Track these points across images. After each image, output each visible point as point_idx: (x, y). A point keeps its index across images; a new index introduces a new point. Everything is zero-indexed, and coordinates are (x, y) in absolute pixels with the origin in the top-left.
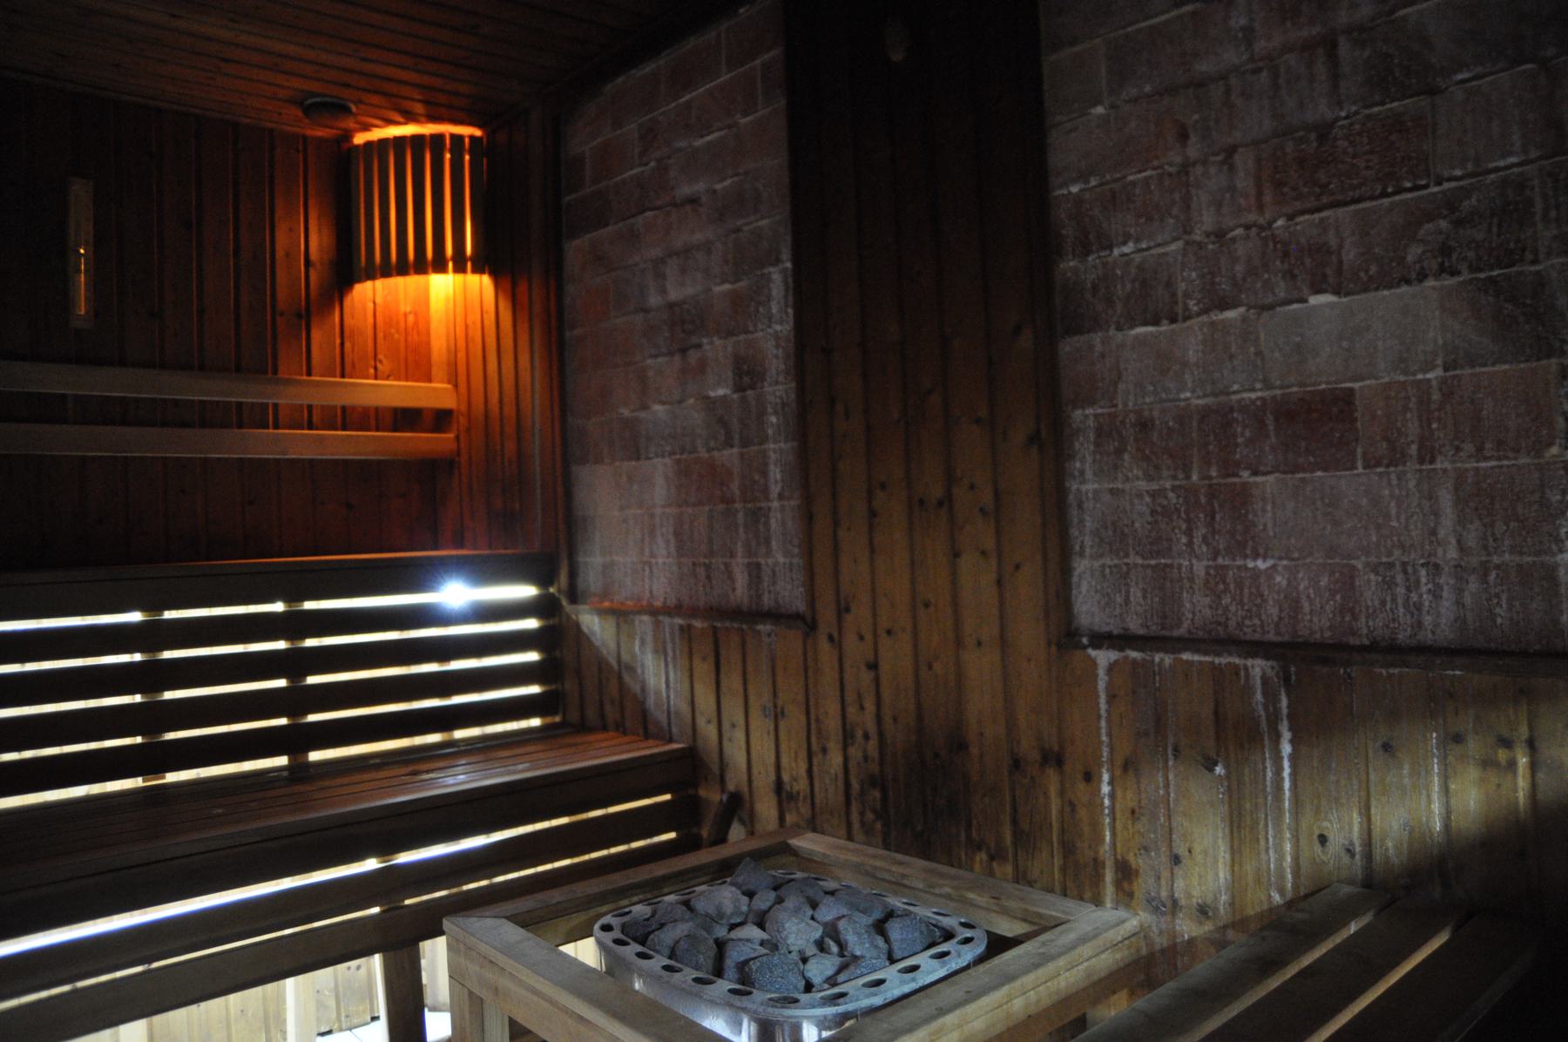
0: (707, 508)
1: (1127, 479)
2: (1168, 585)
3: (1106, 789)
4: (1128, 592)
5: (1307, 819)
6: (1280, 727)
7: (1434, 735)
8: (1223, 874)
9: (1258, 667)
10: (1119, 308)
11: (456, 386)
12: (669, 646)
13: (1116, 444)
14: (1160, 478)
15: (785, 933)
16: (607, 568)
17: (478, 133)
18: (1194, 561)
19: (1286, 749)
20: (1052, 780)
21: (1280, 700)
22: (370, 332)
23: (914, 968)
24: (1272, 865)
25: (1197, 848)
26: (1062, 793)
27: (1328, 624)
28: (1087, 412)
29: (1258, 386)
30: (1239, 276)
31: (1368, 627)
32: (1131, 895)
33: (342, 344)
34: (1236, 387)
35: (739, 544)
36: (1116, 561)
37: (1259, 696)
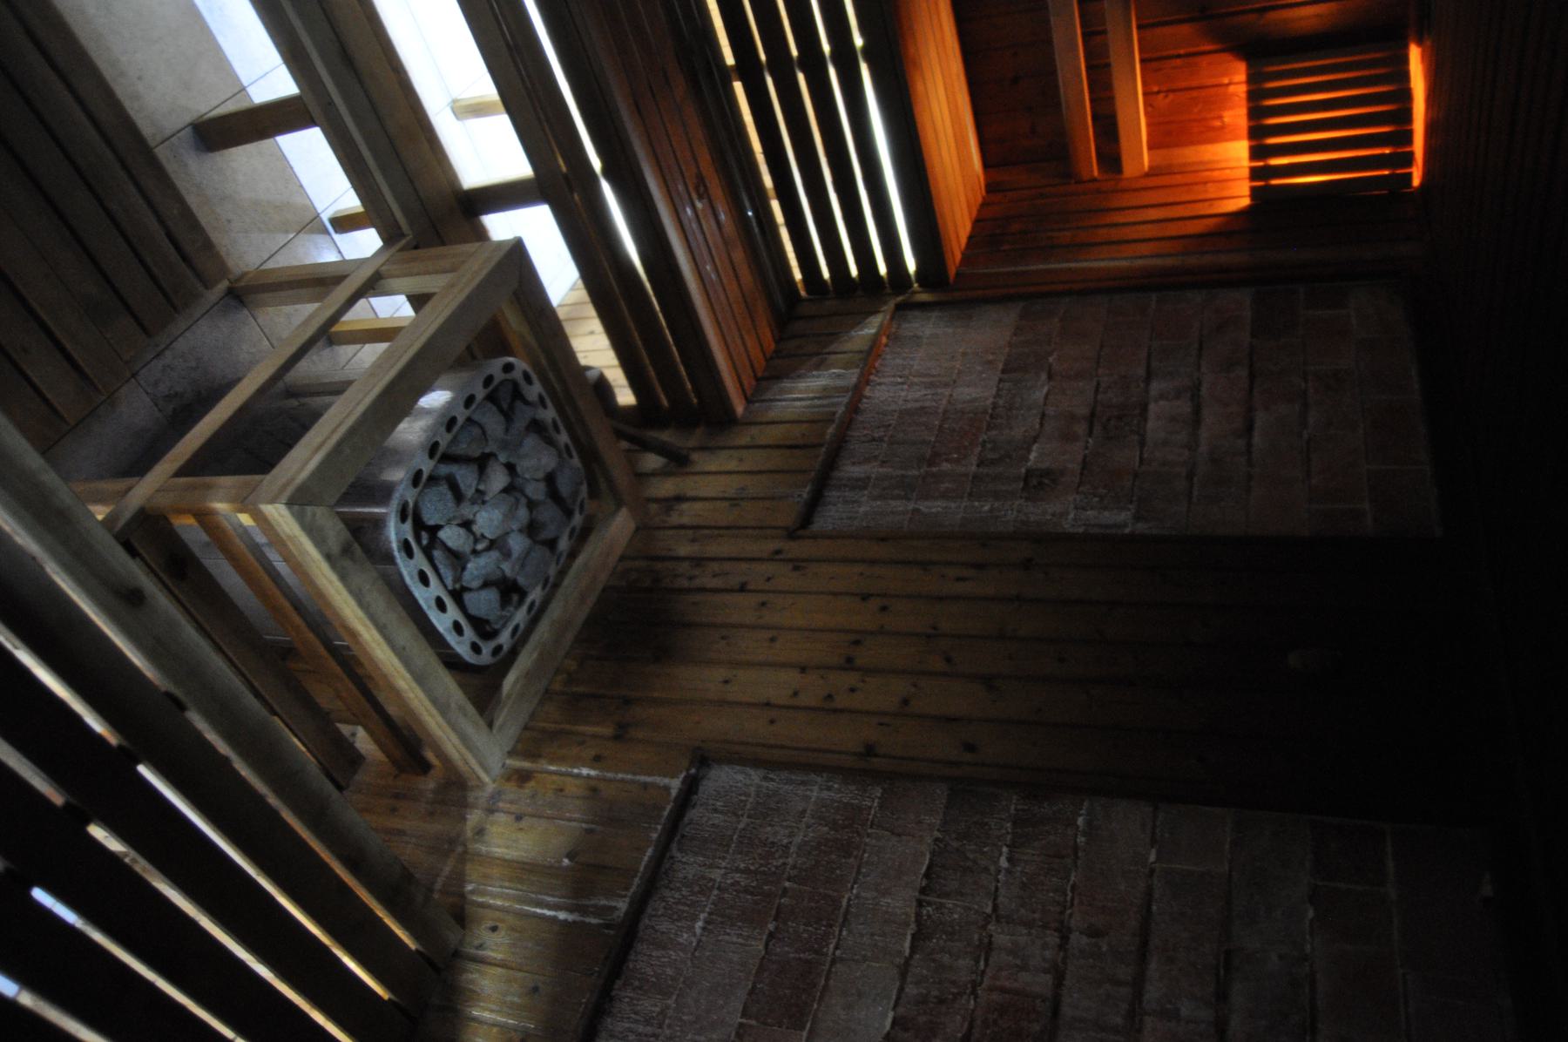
1: (808, 827)
2: (714, 847)
3: (585, 771)
4: (721, 812)
5: (510, 919)
6: (577, 914)
7: (532, 1026)
8: (498, 851)
9: (622, 905)
10: (955, 844)
11: (1147, 175)
12: (825, 402)
13: (840, 822)
14: (798, 855)
16: (917, 339)
17: (1416, 182)
18: (723, 871)
19: (562, 915)
20: (607, 730)
21: (595, 918)
22: (1195, 83)
24: (490, 888)
25: (520, 835)
26: (594, 736)
27: (638, 967)
28: (876, 801)
29: (838, 953)
30: (938, 957)
31: (624, 998)
32: (508, 779)
33: (1179, 56)
34: (844, 933)
35: (890, 470)
36: (748, 806)
37: (603, 902)
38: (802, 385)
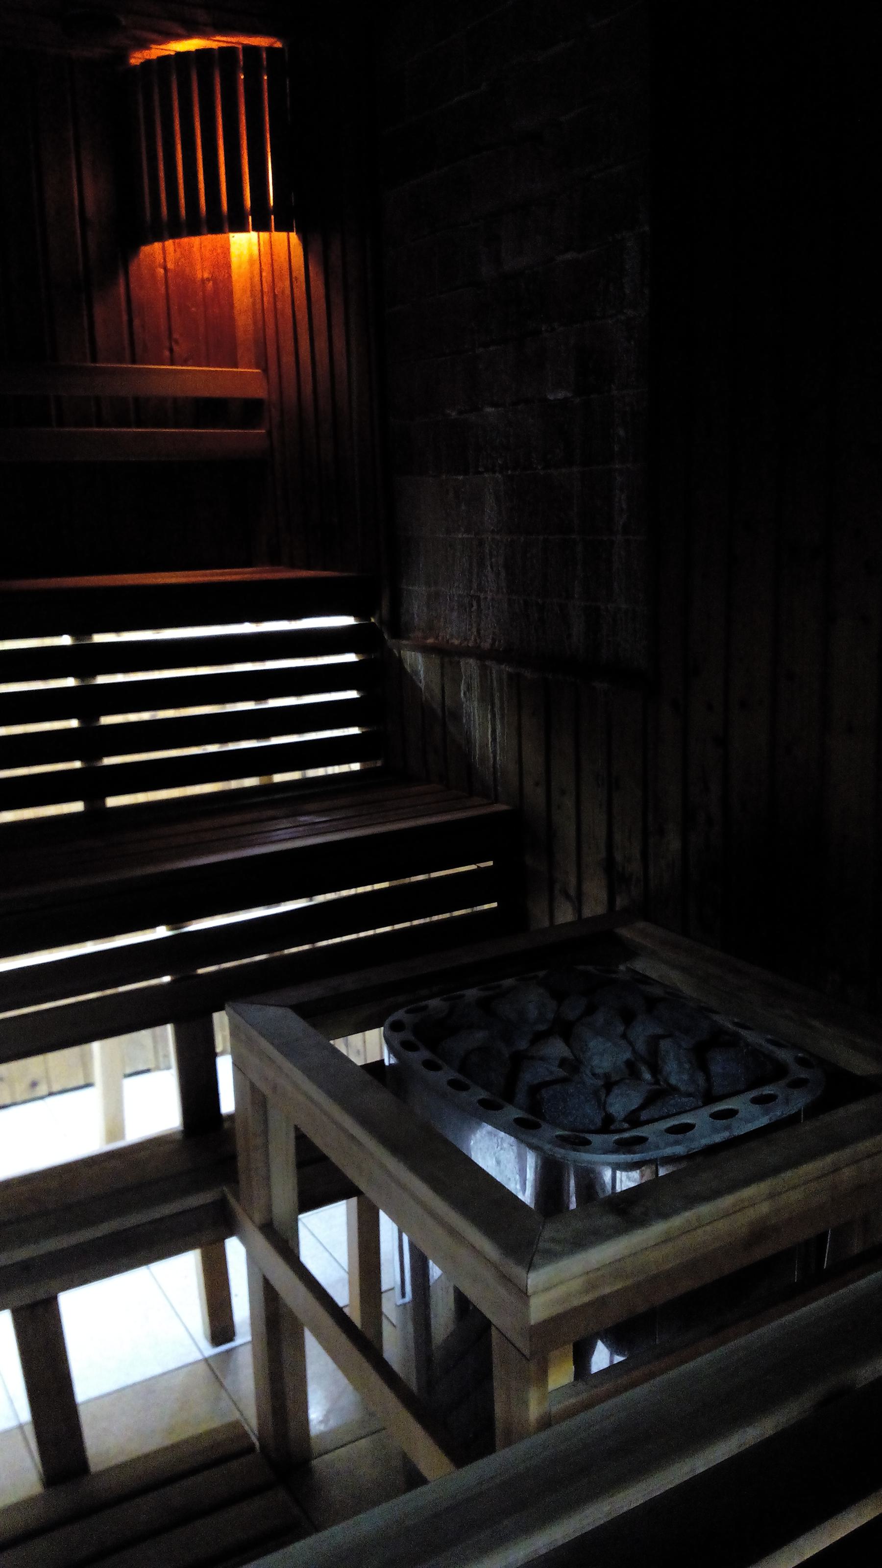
0: (541, 538)
11: (265, 370)
15: (589, 1054)
23: (731, 1114)
38: (477, 734)
